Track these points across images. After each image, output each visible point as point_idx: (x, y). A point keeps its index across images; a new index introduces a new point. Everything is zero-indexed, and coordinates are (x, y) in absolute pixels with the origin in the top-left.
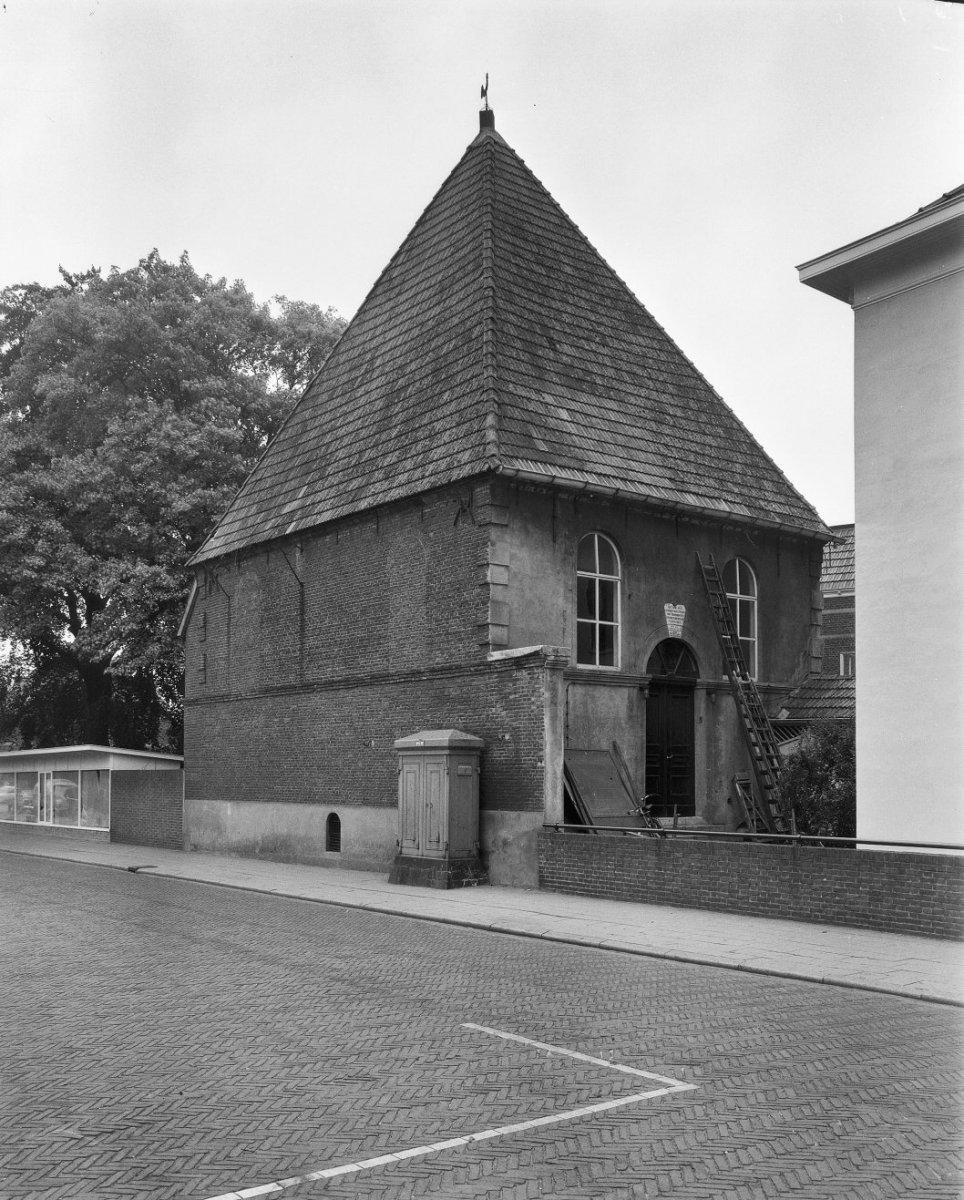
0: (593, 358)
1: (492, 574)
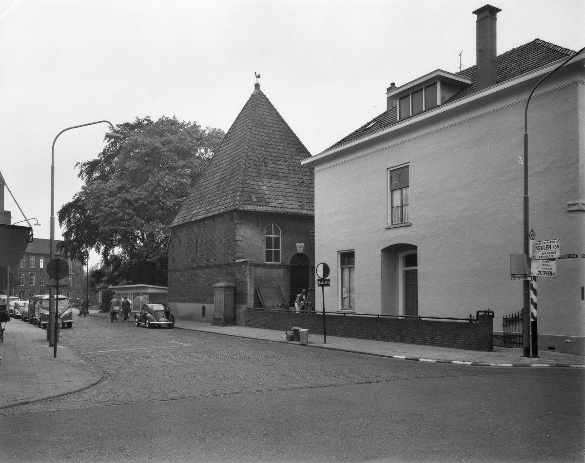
0: (280, 167)
1: (238, 238)
